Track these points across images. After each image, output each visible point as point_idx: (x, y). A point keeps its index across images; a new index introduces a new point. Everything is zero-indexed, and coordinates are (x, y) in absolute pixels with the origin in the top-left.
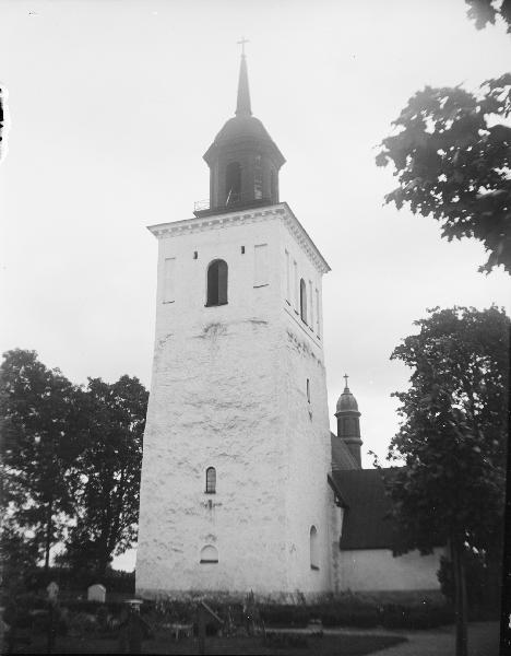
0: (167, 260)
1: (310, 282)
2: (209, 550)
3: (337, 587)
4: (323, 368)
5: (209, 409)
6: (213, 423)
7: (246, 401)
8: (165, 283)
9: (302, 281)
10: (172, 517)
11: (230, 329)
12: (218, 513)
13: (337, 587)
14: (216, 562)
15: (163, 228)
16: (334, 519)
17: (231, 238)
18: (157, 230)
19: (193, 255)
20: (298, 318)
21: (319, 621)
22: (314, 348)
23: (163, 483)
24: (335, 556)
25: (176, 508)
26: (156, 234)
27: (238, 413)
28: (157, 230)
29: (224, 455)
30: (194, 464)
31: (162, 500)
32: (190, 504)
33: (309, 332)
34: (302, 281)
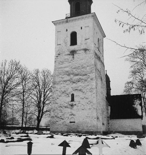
0: (58, 32)
1: (100, 40)
2: (73, 118)
3: (109, 130)
4: (104, 65)
5: (72, 76)
6: (73, 80)
7: (83, 73)
8: (57, 39)
9: (98, 39)
10: (61, 109)
11: (69, 53)
12: (75, 107)
13: (109, 130)
14: (75, 122)
15: (62, 21)
16: (108, 110)
17: (82, 25)
18: (55, 23)
19: (81, 28)
20: (98, 49)
21: (60, 134)
22: (102, 59)
23: (58, 98)
24: (108, 121)
25: (62, 106)
26: (55, 24)
27: (81, 77)
28: (55, 23)
29: (77, 90)
30: (68, 92)
31: (57, 103)
32: (66, 105)
33: (100, 54)
34: (98, 39)
